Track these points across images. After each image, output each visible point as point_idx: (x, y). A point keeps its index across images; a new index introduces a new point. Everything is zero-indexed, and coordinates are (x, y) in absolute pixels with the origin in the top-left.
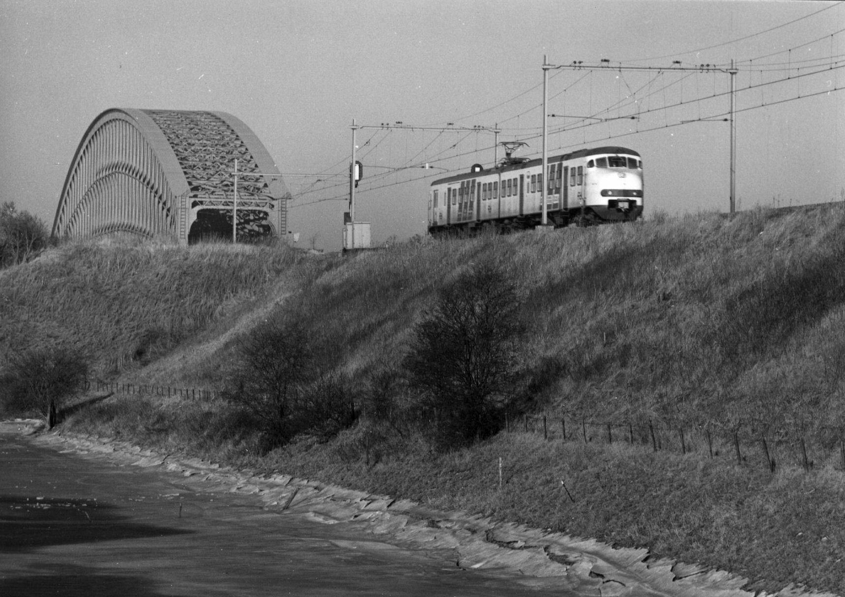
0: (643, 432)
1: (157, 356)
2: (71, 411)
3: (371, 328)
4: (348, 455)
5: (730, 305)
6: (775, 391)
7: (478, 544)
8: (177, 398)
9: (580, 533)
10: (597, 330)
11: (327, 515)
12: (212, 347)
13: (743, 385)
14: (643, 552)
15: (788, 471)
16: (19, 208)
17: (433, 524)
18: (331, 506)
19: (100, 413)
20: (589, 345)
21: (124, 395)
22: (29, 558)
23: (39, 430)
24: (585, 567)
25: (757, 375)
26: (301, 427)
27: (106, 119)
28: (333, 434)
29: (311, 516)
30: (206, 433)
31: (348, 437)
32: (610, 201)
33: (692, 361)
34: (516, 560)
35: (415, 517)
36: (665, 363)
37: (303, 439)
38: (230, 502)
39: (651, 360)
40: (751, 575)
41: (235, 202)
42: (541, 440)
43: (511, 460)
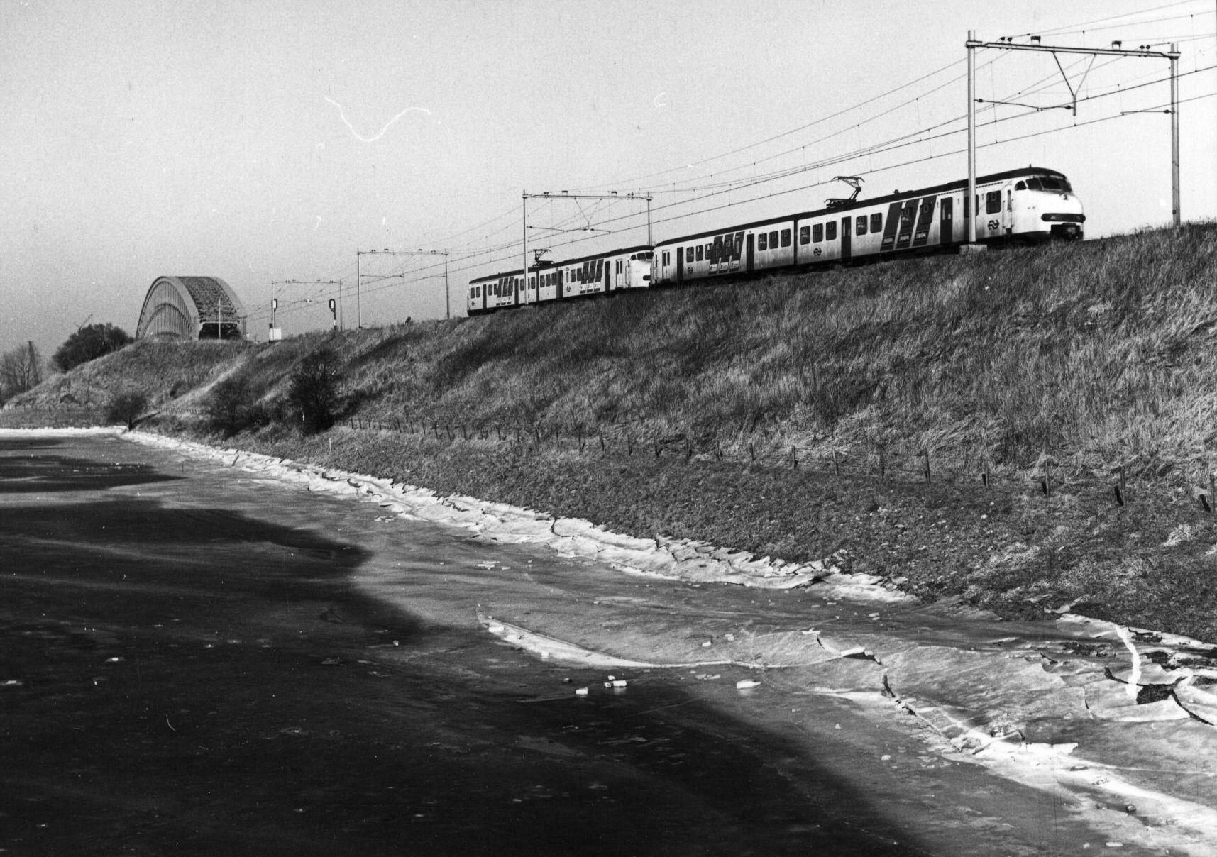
0: (396, 424)
1: (182, 393)
2: (138, 422)
3: (279, 378)
4: (264, 439)
5: (439, 363)
6: (456, 403)
7: (319, 479)
8: (188, 414)
9: (364, 472)
10: (380, 376)
11: (251, 467)
12: (206, 389)
13: (442, 401)
14: (391, 481)
15: (458, 440)
16: (114, 325)
17: (299, 471)
18: (254, 463)
19: (152, 423)
20: (376, 383)
21: (164, 413)
22: (104, 492)
23: (125, 432)
24: (364, 490)
25: (448, 396)
26: (243, 427)
27: (159, 282)
28: (258, 429)
29: (244, 469)
30: (200, 431)
31: (265, 430)
32: (1053, 227)
33: (421, 390)
34: (333, 487)
35: (291, 467)
36: (410, 390)
37: (245, 432)
38: (208, 464)
39: (403, 390)
40: (437, 489)
41: (220, 320)
42: (350, 429)
43: (336, 439)
